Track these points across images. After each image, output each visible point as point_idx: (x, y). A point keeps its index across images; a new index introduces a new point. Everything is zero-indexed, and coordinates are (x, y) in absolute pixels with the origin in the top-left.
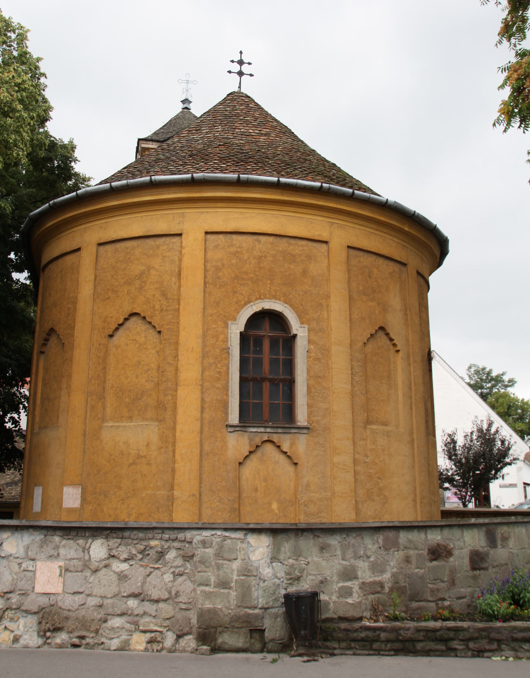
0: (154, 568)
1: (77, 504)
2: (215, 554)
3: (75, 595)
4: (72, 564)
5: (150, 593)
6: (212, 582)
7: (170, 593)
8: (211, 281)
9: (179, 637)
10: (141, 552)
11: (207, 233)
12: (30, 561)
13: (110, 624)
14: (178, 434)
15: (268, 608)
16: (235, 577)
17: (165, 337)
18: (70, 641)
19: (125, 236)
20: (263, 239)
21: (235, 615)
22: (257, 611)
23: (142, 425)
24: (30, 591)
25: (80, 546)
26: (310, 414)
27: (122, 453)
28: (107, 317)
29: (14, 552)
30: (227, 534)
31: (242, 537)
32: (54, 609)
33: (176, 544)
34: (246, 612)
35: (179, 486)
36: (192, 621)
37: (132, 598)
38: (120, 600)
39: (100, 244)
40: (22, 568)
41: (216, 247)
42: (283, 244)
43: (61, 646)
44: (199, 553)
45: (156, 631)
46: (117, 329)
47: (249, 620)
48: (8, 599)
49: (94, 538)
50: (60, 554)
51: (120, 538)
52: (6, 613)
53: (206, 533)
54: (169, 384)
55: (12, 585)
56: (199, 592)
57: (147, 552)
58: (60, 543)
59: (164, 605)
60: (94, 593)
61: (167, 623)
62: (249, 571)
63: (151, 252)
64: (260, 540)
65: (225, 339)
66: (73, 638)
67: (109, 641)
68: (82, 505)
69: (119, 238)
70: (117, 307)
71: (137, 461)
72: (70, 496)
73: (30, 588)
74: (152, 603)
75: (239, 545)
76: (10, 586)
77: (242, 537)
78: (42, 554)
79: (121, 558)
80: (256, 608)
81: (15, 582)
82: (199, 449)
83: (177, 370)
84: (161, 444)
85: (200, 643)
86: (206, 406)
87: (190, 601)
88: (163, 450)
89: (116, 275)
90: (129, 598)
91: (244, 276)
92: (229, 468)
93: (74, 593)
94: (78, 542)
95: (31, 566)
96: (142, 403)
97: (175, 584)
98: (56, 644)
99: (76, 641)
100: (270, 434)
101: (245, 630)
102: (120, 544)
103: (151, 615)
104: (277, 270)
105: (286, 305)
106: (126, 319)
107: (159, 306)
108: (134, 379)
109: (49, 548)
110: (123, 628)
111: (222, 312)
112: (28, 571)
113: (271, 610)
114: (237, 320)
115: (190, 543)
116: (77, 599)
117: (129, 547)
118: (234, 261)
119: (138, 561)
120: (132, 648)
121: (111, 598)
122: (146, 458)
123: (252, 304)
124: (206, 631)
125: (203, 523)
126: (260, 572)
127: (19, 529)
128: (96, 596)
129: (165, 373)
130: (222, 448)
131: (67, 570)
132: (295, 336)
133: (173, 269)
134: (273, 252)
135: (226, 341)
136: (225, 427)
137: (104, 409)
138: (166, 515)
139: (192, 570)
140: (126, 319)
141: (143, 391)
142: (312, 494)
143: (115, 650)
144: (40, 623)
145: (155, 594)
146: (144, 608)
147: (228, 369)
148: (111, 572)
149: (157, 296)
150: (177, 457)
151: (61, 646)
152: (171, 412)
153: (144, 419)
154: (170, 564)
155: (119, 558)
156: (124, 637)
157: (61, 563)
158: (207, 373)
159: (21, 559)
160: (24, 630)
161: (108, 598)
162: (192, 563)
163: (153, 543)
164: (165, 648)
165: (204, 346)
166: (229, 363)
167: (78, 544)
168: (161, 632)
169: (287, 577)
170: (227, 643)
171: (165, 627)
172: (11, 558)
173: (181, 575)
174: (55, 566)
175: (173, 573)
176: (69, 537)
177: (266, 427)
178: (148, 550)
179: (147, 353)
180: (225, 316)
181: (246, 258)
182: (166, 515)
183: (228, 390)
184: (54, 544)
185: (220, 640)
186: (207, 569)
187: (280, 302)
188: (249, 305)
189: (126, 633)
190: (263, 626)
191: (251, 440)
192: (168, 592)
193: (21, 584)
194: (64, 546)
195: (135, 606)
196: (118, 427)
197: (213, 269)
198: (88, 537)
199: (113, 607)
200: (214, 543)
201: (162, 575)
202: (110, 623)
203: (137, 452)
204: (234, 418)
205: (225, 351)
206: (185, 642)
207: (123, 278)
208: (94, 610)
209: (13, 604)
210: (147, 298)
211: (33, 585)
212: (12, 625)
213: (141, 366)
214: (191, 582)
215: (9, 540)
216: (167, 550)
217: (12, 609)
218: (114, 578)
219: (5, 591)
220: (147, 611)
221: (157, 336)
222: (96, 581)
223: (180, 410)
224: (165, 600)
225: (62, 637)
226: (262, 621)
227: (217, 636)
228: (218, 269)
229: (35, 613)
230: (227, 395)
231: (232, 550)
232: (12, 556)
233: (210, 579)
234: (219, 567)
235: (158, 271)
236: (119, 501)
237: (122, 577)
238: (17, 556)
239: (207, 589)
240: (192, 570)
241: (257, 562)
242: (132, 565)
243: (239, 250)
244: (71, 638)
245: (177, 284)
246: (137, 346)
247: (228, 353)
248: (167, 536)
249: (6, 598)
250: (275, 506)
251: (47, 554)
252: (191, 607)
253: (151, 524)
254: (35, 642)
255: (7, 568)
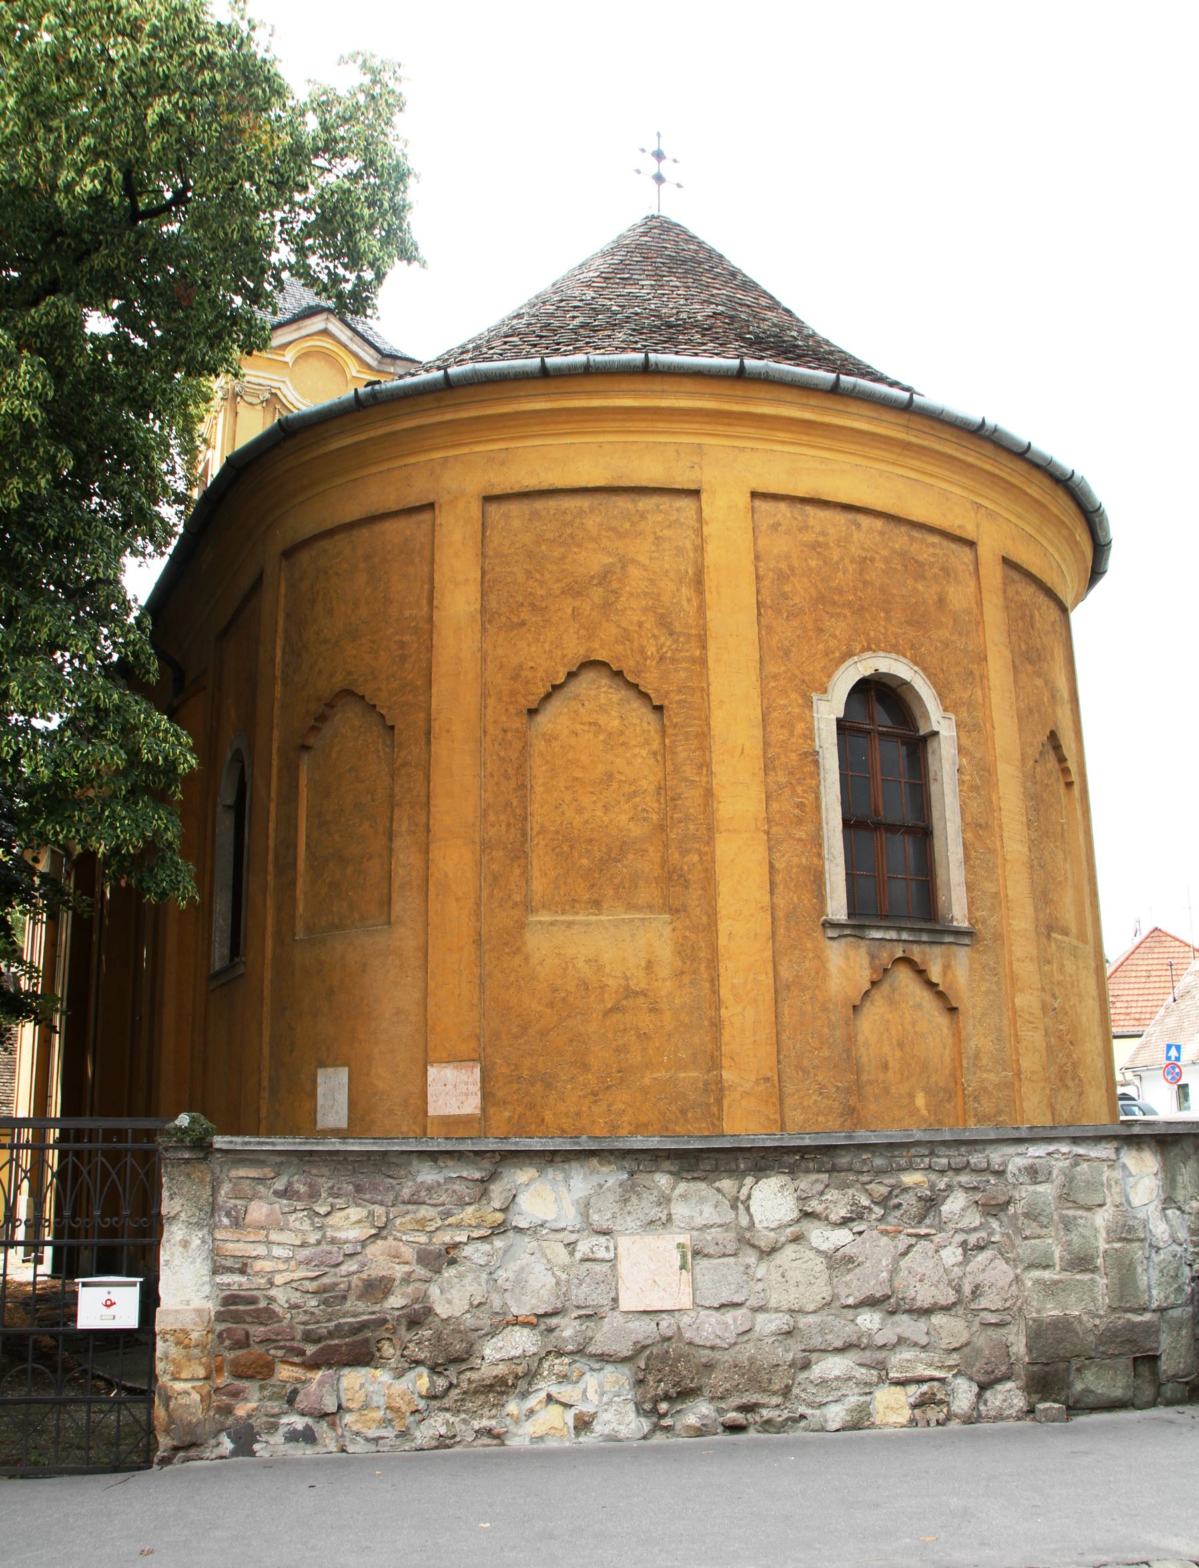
0: (917, 1236)
1: (471, 1105)
2: (1060, 1197)
3: (723, 1310)
4: (709, 1238)
5: (911, 1293)
6: (1057, 1260)
7: (958, 1290)
8: (769, 602)
9: (983, 1387)
10: (883, 1202)
11: (754, 495)
12: (596, 1237)
13: (817, 1371)
14: (722, 941)
15: (1166, 1309)
16: (1103, 1246)
17: (675, 720)
18: (721, 1419)
19: (560, 484)
20: (865, 521)
21: (1108, 1329)
22: (1147, 1317)
23: (632, 920)
24: (606, 1309)
25: (724, 1195)
26: (971, 903)
27: (585, 985)
28: (521, 666)
29: (550, 1216)
30: (1081, 1150)
31: (1113, 1157)
32: (672, 1348)
33: (964, 1178)
34: (1129, 1320)
35: (732, 1058)
36: (1013, 1349)
37: (866, 1309)
38: (836, 1316)
39: (488, 499)
40: (578, 1255)
41: (775, 527)
42: (900, 539)
43: (700, 1431)
44: (1023, 1195)
45: (932, 1379)
46: (548, 697)
47: (1134, 1337)
48: (551, 1330)
49: (761, 1174)
50: (674, 1217)
51: (826, 1171)
52: (546, 1365)
53: (1036, 1151)
54: (692, 827)
55: (558, 1297)
56: (1029, 1284)
57: (896, 1201)
58: (673, 1189)
59: (944, 1320)
60: (773, 1303)
61: (954, 1359)
62: (1131, 1229)
63: (628, 525)
64: (1143, 1160)
65: (808, 733)
66: (727, 1411)
67: (817, 1412)
68: (484, 1109)
69: (545, 486)
70: (547, 646)
71: (624, 1002)
72: (449, 1087)
73: (606, 1301)
74: (915, 1317)
75: (1106, 1173)
76: (553, 1299)
77: (1113, 1157)
78: (629, 1219)
79: (833, 1217)
80: (1145, 1310)
81: (564, 1289)
82: (771, 975)
83: (709, 794)
84: (680, 963)
85: (1035, 1397)
86: (778, 878)
87: (1007, 1305)
88: (686, 979)
89: (538, 571)
90: (860, 1310)
91: (836, 598)
92: (833, 1019)
93: (723, 1306)
94: (717, 1184)
95: (603, 1249)
96: (625, 870)
97: (968, 1269)
98: (689, 1427)
99: (733, 1416)
100: (907, 946)
101: (1125, 1362)
102: (827, 1186)
103: (916, 1344)
104: (895, 591)
105: (916, 668)
106: (571, 675)
107: (654, 649)
108: (598, 813)
109: (644, 1203)
110: (850, 1379)
111: (797, 673)
112: (594, 1260)
113: (1170, 1312)
114: (829, 690)
115: (1000, 1173)
116: (730, 1321)
117: (850, 1192)
118: (813, 563)
119: (875, 1224)
120: (878, 1423)
121: (815, 1312)
122: (645, 995)
123: (856, 658)
124: (1046, 1369)
125: (1031, 1128)
126: (1150, 1231)
127: (558, 1159)
128: (777, 1310)
129: (679, 802)
130: (817, 973)
131: (696, 1253)
132: (935, 734)
133: (683, 568)
134: (885, 553)
135: (809, 735)
136: (820, 928)
137: (527, 882)
138: (704, 1125)
139: (1008, 1235)
140: (571, 675)
141: (624, 843)
142: (985, 1075)
143: (838, 1430)
144: (640, 1382)
145: (924, 1296)
146: (899, 1330)
147: (818, 798)
148: (808, 1252)
149: (648, 625)
150: (724, 993)
151: (700, 1432)
152: (700, 892)
153: (631, 907)
154: (950, 1225)
155: (827, 1218)
156: (853, 1400)
157: (684, 1238)
158: (775, 806)
159: (572, 1232)
160: (600, 1401)
161: (808, 1313)
162: (1005, 1219)
163: (909, 1179)
164: (956, 1416)
165: (766, 745)
166: (818, 786)
167: (718, 1190)
168: (942, 1380)
169: (1194, 1238)
170: (1092, 1392)
171: (951, 1367)
172: (544, 1232)
173: (981, 1248)
174: (666, 1246)
175: (964, 1244)
176: (695, 1175)
177: (900, 929)
178: (897, 1196)
179: (628, 755)
180: (803, 681)
181: (836, 558)
182: (704, 1125)
183: (820, 845)
184: (655, 1193)
185: (1079, 1386)
186: (1043, 1232)
187: (905, 661)
188: (850, 662)
189: (856, 1390)
190: (1157, 1349)
191: (873, 957)
192: (954, 1288)
193: (580, 1294)
194: (683, 1197)
195: (875, 1326)
196: (570, 924)
197: (771, 574)
198: (744, 1174)
199: (822, 1332)
200: (1055, 1172)
201: (937, 1251)
202: (816, 1371)
203: (623, 982)
204: (837, 907)
205: (810, 758)
206: (1000, 1397)
207: (559, 580)
208: (776, 1344)
209: (565, 1340)
210: (625, 630)
211: (613, 1295)
212: (565, 1392)
213: (615, 785)
214: (1007, 1263)
215: (532, 1187)
216: (945, 1194)
217: (560, 1354)
218: (819, 1264)
219: (541, 1311)
220: (905, 1335)
221: (650, 716)
222: (775, 1276)
223: (724, 889)
224: (946, 1309)
225: (698, 1411)
226: (1157, 1336)
227: (1071, 1378)
228: (782, 577)
229: (625, 1360)
230: (820, 855)
231: (1093, 1185)
232: (547, 1225)
233: (1052, 1254)
234: (1068, 1225)
235: (646, 570)
236: (585, 1097)
237: (838, 1262)
238: (562, 1225)
239: (1046, 1275)
240: (1008, 1235)
241: (1144, 1209)
242: (860, 1233)
243: (821, 539)
244: (721, 1412)
245: (695, 603)
246: (602, 737)
247: (816, 763)
248: (944, 1161)
249: (543, 1327)
250: (920, 1101)
251: (642, 1217)
252: (1009, 1318)
253: (909, 1136)
254: (632, 1426)
255: (538, 1255)
